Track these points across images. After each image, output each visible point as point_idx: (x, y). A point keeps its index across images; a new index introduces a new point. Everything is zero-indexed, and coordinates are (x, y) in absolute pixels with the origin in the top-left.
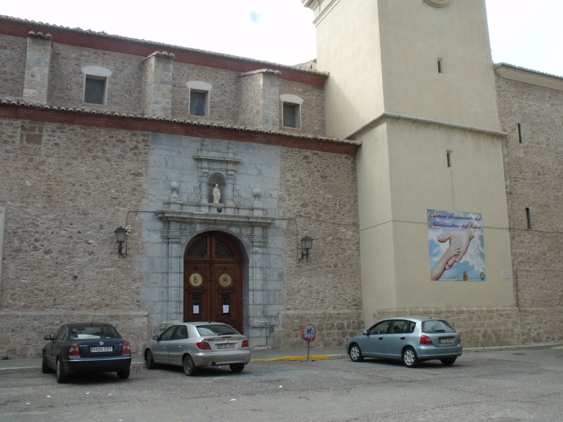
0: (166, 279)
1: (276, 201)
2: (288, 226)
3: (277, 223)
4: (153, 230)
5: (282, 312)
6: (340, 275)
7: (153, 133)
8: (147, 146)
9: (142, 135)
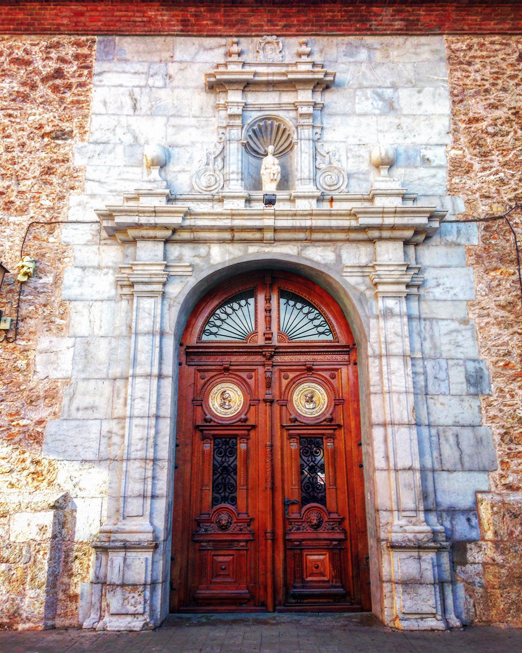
0: (122, 395)
1: (443, 174)
2: (484, 239)
4: (94, 267)
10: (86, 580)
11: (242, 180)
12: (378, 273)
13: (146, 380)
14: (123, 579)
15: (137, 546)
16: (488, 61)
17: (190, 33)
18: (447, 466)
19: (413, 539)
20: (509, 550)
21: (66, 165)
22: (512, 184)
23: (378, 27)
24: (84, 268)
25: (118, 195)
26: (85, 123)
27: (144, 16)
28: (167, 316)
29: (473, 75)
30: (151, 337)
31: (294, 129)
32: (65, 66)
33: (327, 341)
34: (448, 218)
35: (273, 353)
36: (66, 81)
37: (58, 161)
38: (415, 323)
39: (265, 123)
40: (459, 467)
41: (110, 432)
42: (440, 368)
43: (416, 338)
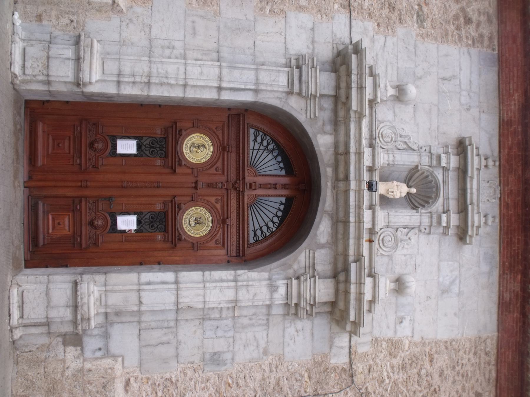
1: (390, 334)
2: (335, 369)
3: (342, 341)
4: (313, 38)
5: (118, 366)
7: (496, 56)
9: (491, 33)
10: (53, 29)
11: (388, 164)
12: (308, 280)
13: (216, 77)
14: (53, 58)
15: (78, 69)
16: (477, 368)
17: (502, 127)
18: (144, 334)
19: (83, 302)
20: (76, 381)
21: (398, 22)
22: (379, 390)
23: (505, 280)
24: (313, 29)
25: (374, 60)
26: (431, 39)
27: (513, 90)
28: (271, 95)
29: (466, 357)
30: (254, 82)
31: (429, 210)
32: (474, 27)
33: (248, 237)
34: (354, 338)
35: (238, 189)
36: (462, 26)
37: (400, 15)
39: (433, 187)
40: (143, 344)
41: (174, 48)
42: (226, 331)
43: (253, 311)
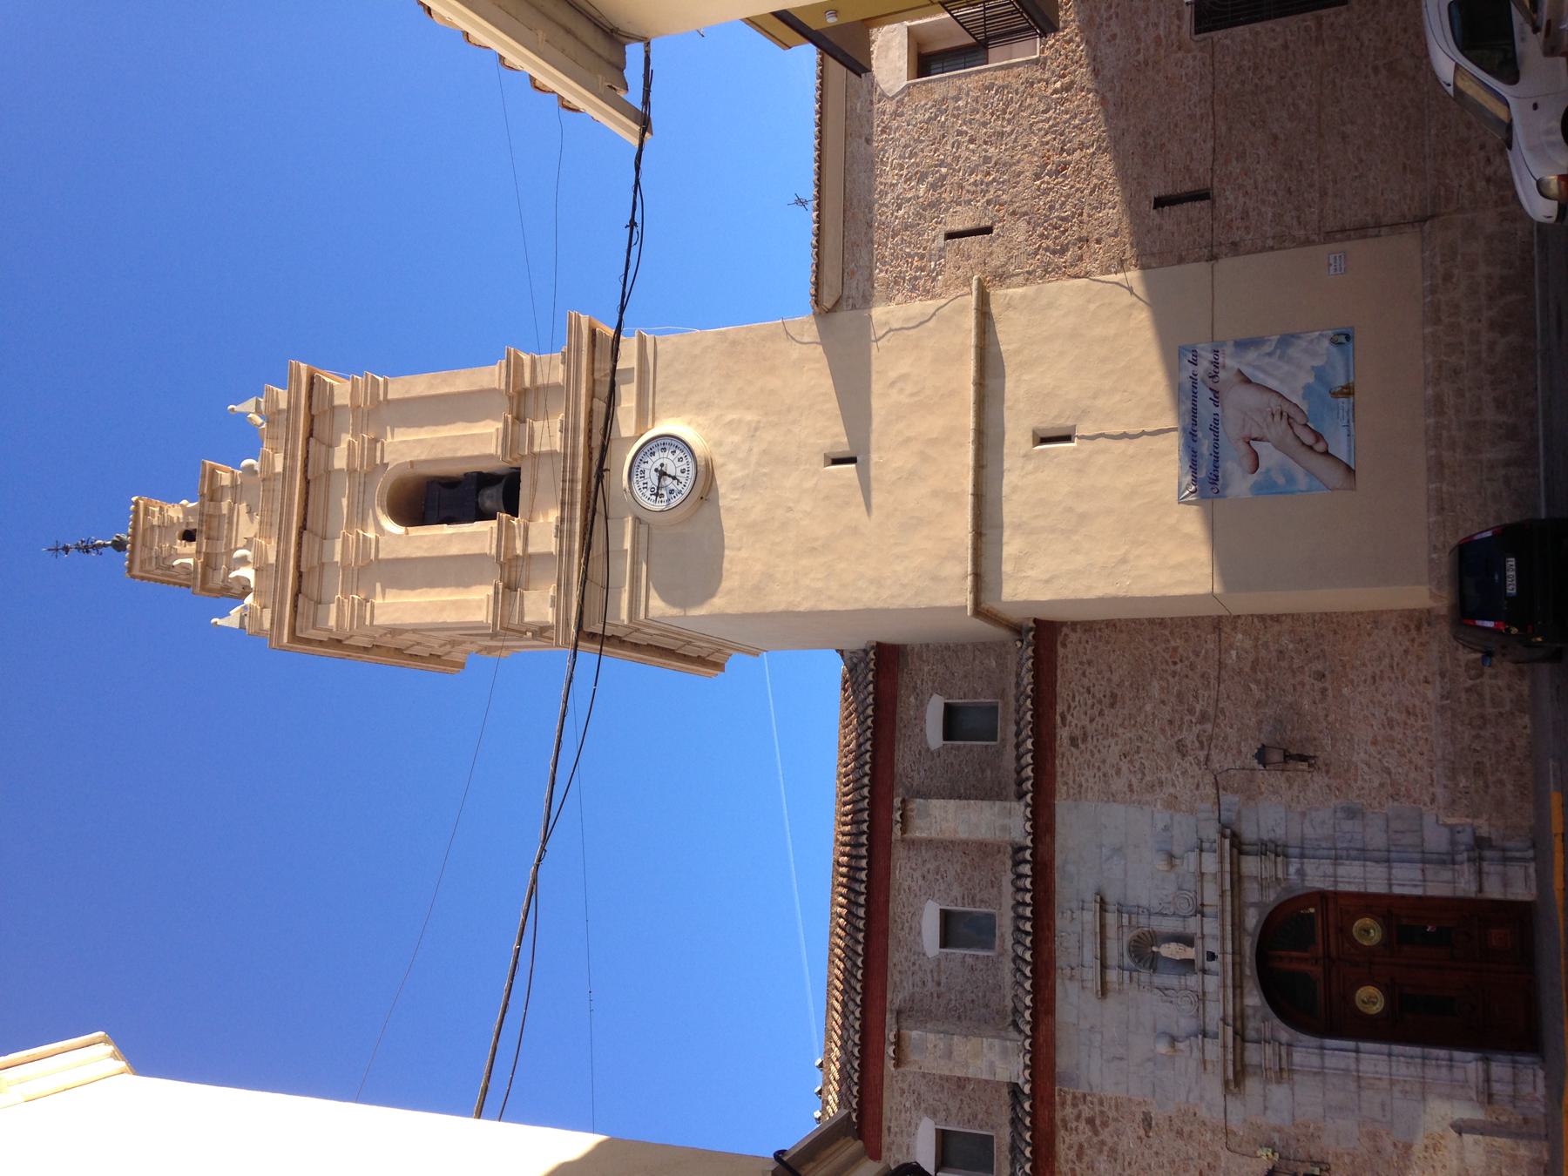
0: (1372, 1081)
1: (1177, 817)
2: (1235, 792)
4: (1264, 1100)
6: (1344, 666)
8: (1084, 1096)
24: (1266, 1108)
38: (1307, 852)
41: (1402, 1092)
